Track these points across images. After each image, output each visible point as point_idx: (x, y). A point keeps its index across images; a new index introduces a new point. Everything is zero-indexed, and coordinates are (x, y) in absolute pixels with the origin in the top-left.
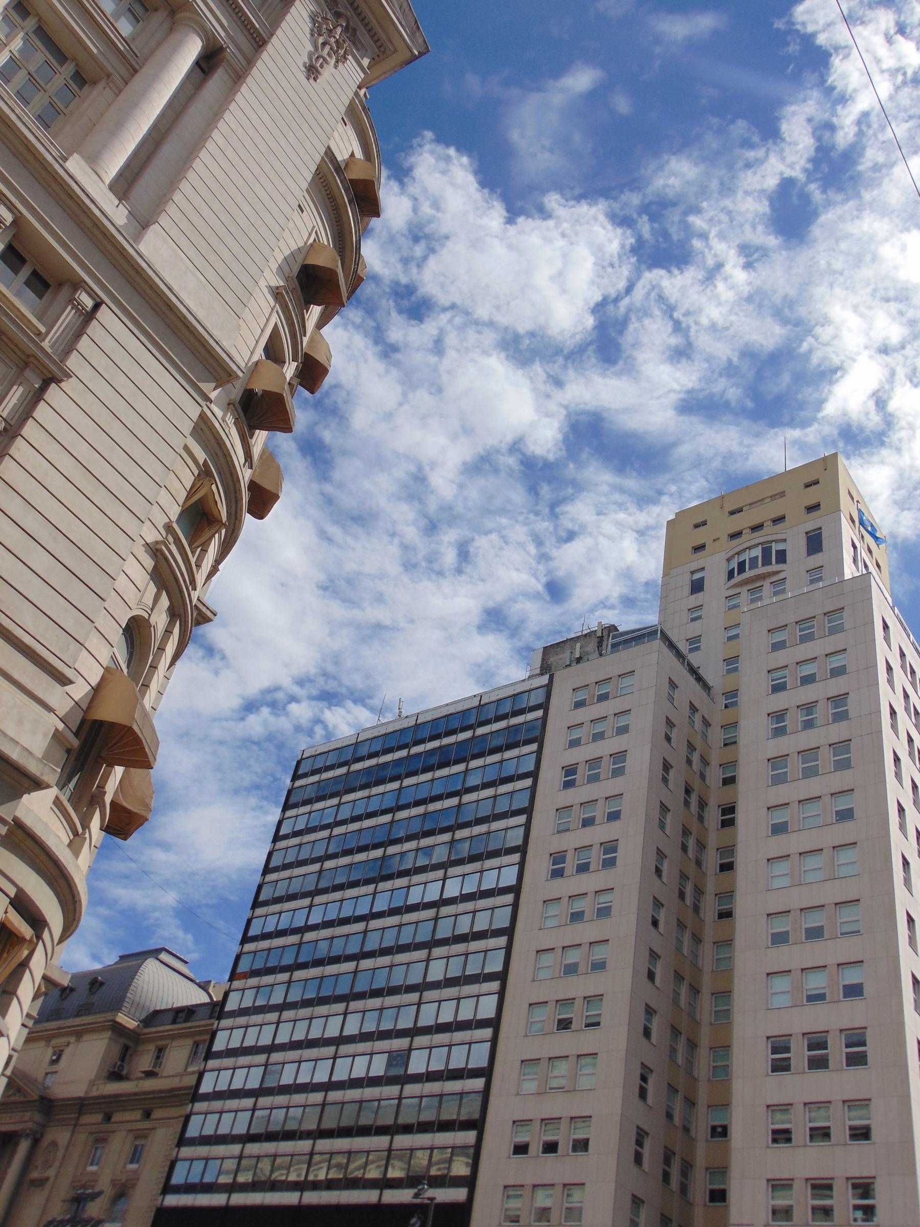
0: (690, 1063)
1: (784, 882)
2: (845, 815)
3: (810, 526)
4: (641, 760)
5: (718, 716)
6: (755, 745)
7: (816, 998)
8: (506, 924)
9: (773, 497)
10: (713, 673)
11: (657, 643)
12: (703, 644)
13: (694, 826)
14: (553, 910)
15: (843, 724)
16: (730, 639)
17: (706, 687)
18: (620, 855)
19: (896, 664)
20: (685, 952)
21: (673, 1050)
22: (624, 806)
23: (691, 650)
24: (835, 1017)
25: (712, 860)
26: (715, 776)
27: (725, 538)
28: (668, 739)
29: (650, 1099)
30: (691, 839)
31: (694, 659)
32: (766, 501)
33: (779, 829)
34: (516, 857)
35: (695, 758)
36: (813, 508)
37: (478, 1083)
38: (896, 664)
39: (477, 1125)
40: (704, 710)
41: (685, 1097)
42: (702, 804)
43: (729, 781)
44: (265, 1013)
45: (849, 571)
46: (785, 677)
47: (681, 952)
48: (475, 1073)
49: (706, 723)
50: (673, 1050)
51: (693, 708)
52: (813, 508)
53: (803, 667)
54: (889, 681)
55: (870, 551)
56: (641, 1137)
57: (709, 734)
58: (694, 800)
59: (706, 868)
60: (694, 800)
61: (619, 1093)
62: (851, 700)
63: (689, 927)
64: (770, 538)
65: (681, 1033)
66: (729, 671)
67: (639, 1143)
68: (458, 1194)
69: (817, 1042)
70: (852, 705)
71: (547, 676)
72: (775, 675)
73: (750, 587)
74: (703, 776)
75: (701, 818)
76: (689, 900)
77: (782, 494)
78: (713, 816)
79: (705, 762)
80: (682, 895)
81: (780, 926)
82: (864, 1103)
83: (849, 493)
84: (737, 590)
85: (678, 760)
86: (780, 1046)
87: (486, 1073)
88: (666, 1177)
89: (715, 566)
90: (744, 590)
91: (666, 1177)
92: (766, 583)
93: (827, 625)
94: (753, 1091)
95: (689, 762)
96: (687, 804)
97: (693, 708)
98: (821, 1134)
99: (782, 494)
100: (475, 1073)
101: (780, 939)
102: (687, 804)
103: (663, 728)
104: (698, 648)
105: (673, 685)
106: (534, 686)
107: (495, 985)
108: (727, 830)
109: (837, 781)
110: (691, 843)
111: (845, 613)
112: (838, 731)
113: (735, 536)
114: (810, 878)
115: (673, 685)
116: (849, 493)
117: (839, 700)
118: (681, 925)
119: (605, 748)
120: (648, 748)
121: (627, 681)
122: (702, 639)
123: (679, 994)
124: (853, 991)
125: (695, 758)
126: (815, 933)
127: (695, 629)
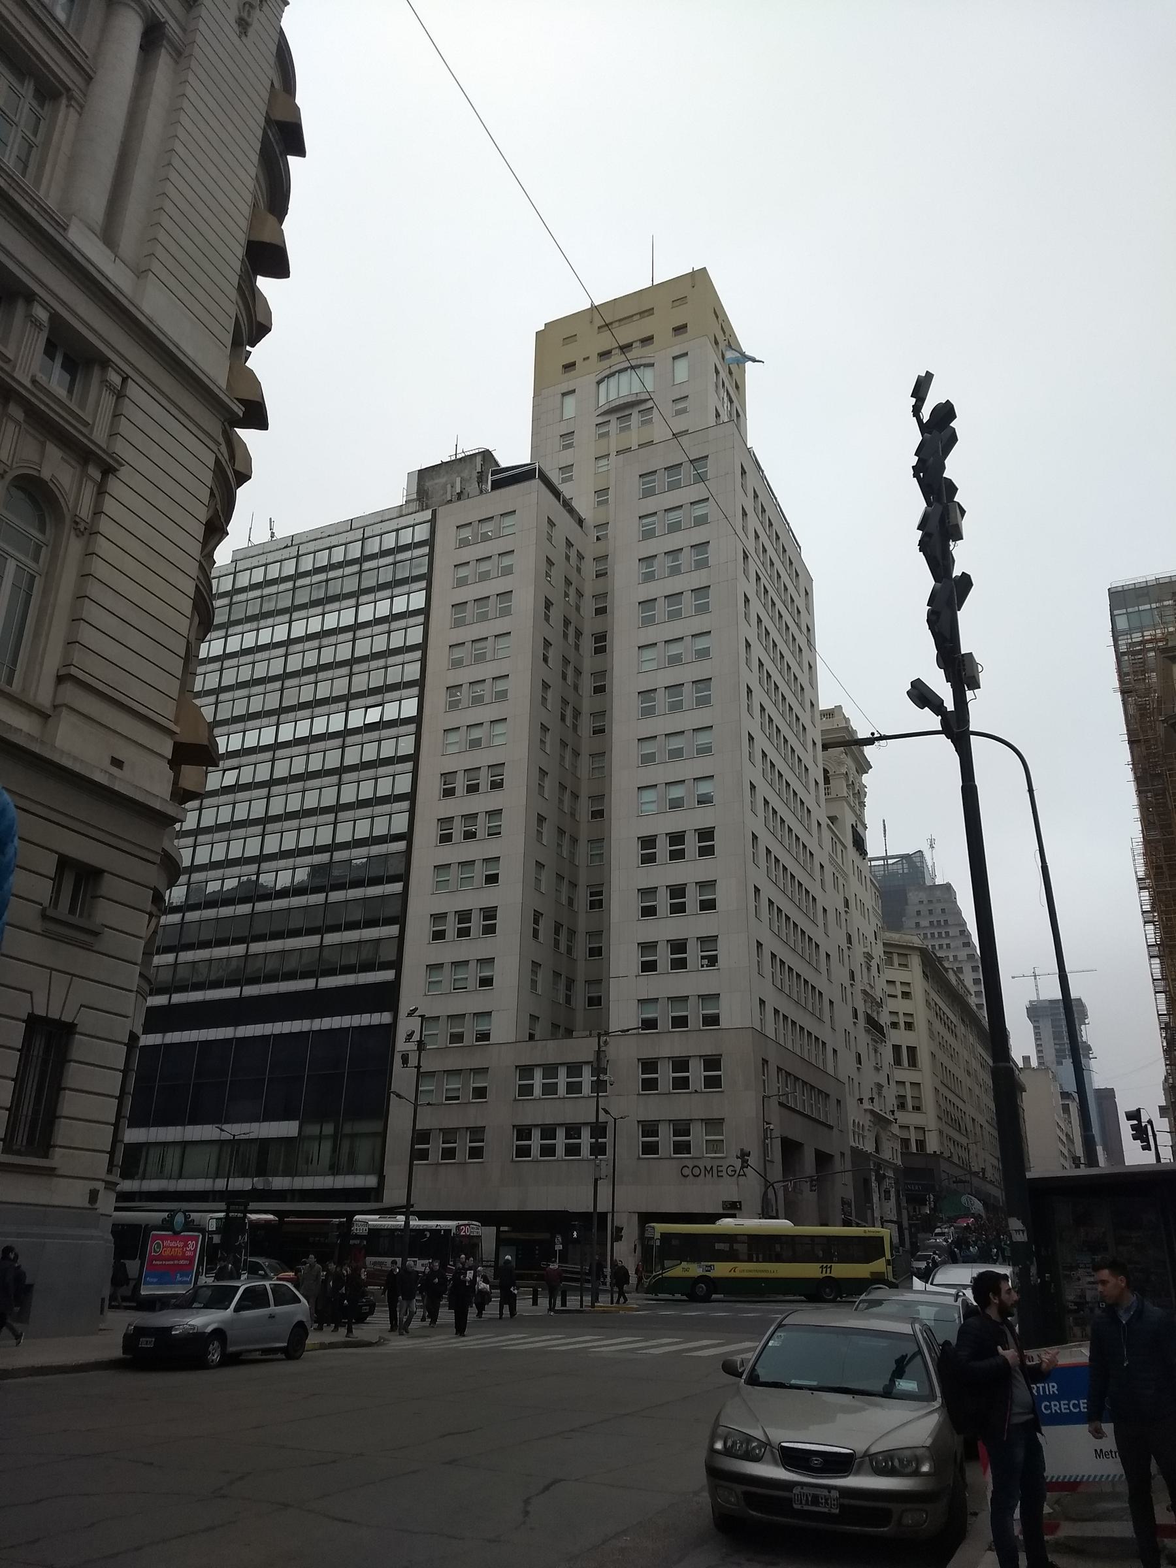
0: (572, 854)
1: (652, 666)
4: (525, 601)
5: (591, 549)
6: (627, 588)
7: (676, 804)
8: (411, 750)
10: (584, 505)
11: (536, 483)
14: (453, 737)
16: (601, 436)
17: (580, 522)
18: (499, 922)
21: (562, 758)
22: (502, 870)
23: (564, 480)
24: (690, 821)
25: (587, 684)
26: (589, 606)
29: (541, 938)
30: (569, 711)
31: (566, 490)
32: (635, 318)
34: (421, 619)
35: (572, 591)
37: (401, 845)
39: (400, 919)
40: (578, 545)
42: (579, 634)
43: (601, 611)
44: (183, 1124)
48: (397, 838)
49: (581, 557)
50: (562, 758)
51: (569, 544)
55: (730, 373)
56: (537, 916)
58: (571, 631)
61: (519, 887)
62: (711, 547)
63: (569, 747)
67: (536, 922)
68: (388, 975)
69: (677, 838)
71: (430, 512)
72: (645, 521)
73: (619, 415)
74: (579, 570)
76: (569, 680)
77: (650, 311)
78: (587, 644)
79: (580, 594)
80: (564, 677)
82: (712, 884)
84: (605, 419)
86: (648, 842)
87: (408, 836)
88: (557, 943)
90: (613, 418)
91: (557, 943)
92: (635, 412)
94: (626, 878)
95: (568, 558)
97: (569, 544)
98: (680, 1022)
99: (650, 311)
100: (397, 838)
101: (647, 759)
103: (544, 566)
104: (570, 479)
105: (551, 523)
106: (417, 521)
107: (409, 766)
109: (695, 492)
110: (569, 713)
111: (709, 461)
113: (605, 355)
115: (551, 523)
118: (564, 744)
119: (492, 588)
120: (532, 589)
121: (508, 521)
124: (704, 800)
125: (573, 554)
126: (676, 754)
127: (566, 457)
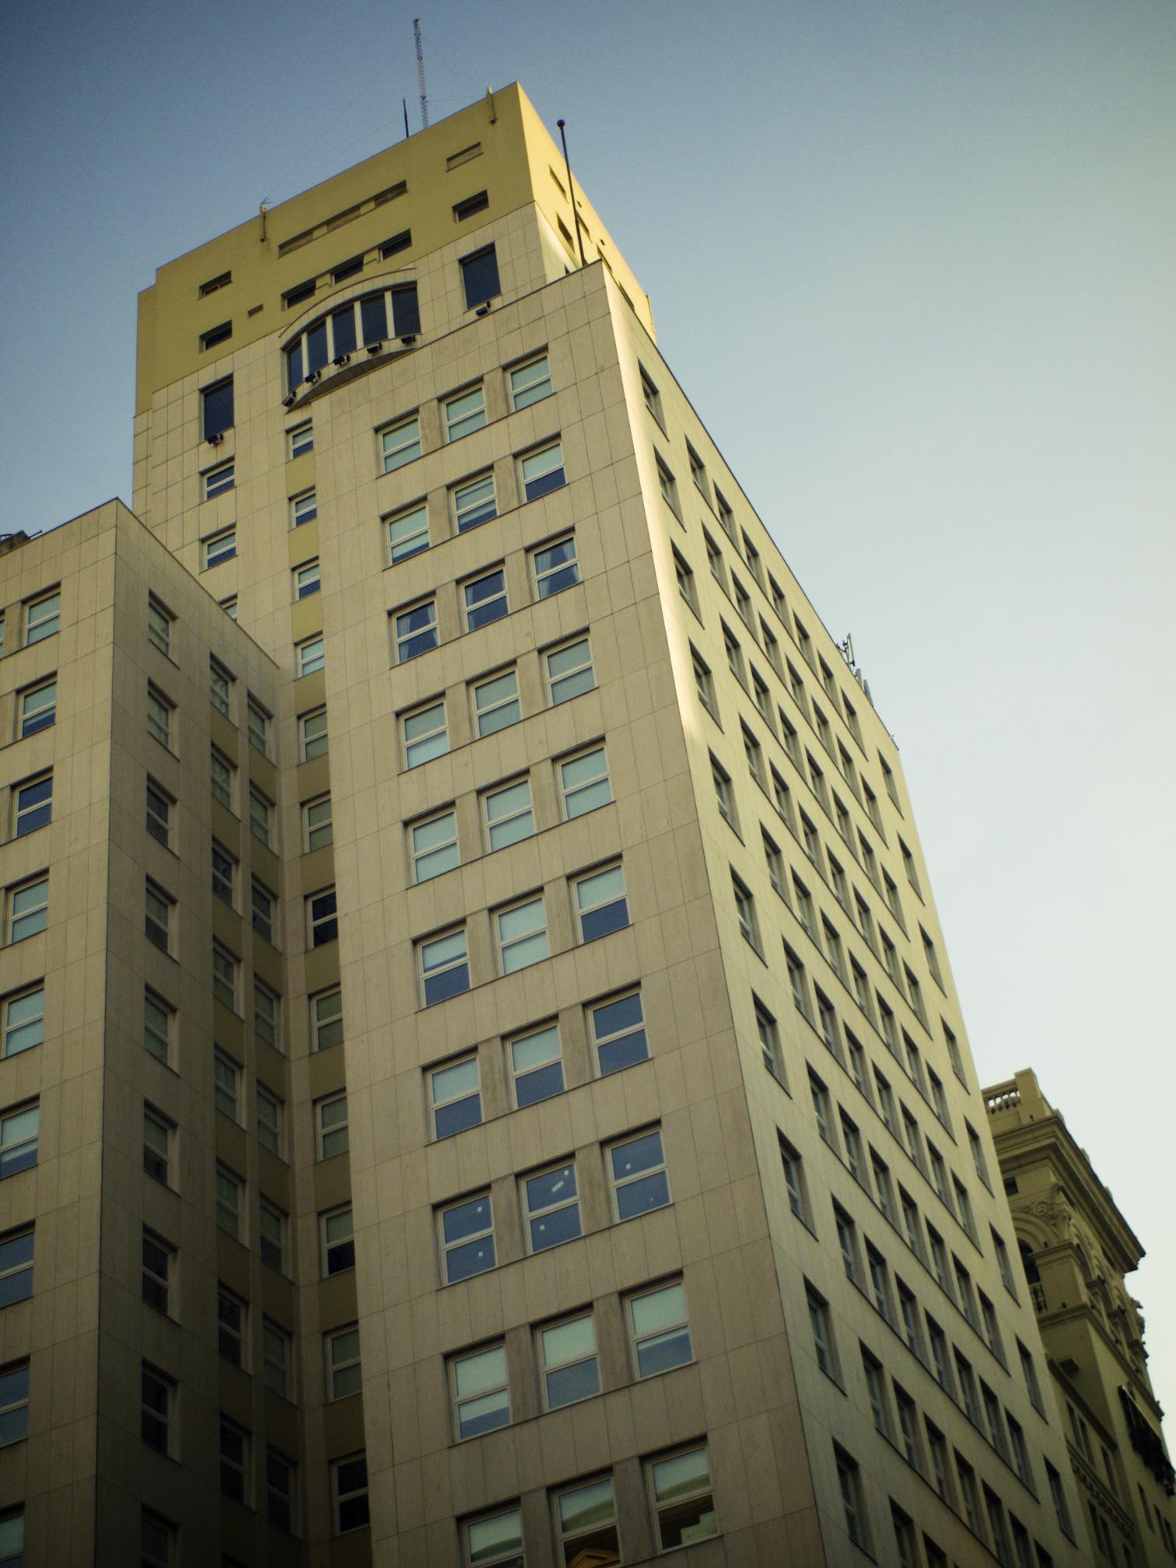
2: (608, 921)
3: (468, 245)
9: (381, 199)
12: (239, 542)
13: (246, 943)
15: (568, 596)
16: (298, 452)
19: (736, 763)
20: (243, 1119)
27: (274, 302)
28: (157, 935)
33: (447, 986)
36: (472, 206)
38: (758, 879)
41: (266, 1317)
45: (558, 255)
46: (464, 955)
47: (233, 1121)
49: (260, 711)
52: (472, 206)
53: (509, 920)
54: (769, 1064)
57: (269, 735)
59: (284, 941)
60: (239, 882)
64: (379, 284)
65: (243, 1181)
66: (302, 520)
70: (583, 557)
75: (262, 929)
81: (456, 1086)
83: (552, 173)
85: (190, 783)
89: (257, 370)
93: (614, 1184)
96: (222, 891)
102: (222, 891)
103: (138, 907)
108: (324, 949)
112: (557, 616)
113: (296, 295)
114: (518, 959)
116: (552, 173)
117: (554, 545)
122: (236, 463)
123: (234, 1217)
